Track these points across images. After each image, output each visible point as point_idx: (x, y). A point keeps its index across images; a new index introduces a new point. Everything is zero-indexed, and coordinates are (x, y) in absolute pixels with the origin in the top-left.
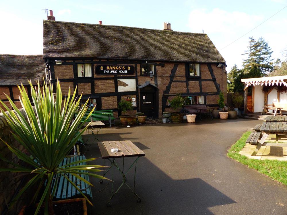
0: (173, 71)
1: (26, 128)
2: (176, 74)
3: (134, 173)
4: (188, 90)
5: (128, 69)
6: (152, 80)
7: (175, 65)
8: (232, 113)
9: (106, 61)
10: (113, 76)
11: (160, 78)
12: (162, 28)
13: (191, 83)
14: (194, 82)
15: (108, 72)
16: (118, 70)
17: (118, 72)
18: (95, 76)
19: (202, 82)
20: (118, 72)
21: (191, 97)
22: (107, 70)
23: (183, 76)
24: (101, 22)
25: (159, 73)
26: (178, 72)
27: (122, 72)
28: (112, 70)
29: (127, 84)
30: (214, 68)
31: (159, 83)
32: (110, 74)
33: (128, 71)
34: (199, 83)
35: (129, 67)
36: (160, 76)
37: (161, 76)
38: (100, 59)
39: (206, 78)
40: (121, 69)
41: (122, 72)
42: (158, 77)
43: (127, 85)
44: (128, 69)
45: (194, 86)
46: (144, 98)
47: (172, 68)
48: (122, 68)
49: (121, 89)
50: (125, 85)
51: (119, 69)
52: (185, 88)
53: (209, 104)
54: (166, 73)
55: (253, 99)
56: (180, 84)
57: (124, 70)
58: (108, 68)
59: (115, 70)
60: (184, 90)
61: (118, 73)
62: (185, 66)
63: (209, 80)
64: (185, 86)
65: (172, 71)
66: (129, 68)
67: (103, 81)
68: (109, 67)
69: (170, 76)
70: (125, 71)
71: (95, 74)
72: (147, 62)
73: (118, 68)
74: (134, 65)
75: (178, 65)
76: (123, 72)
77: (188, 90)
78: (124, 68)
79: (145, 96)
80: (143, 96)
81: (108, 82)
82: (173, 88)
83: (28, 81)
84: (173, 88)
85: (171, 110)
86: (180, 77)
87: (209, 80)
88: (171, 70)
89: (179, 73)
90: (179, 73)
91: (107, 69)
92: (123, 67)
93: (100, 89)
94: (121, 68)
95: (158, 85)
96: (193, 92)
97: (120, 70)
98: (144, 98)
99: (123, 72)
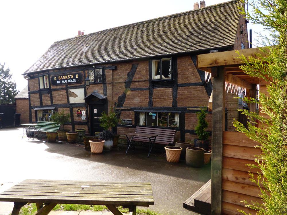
0: (131, 75)
1: (206, 80)
2: (136, 78)
4: (151, 103)
5: (77, 77)
6: (233, 55)
11: (109, 85)
13: (158, 91)
14: (162, 89)
15: (59, 82)
17: (61, 82)
18: (52, 87)
19: (179, 89)
21: (155, 115)
22: (59, 80)
23: (144, 81)
25: (109, 79)
26: (138, 75)
28: (63, 80)
29: (77, 95)
31: (109, 92)
32: (62, 84)
33: (77, 79)
34: (173, 91)
36: (109, 84)
37: (110, 83)
39: (189, 82)
40: (70, 79)
42: (107, 85)
43: (77, 96)
44: (77, 77)
45: (162, 96)
46: (95, 111)
47: (129, 70)
49: (72, 100)
50: (75, 96)
52: (146, 98)
53: (189, 129)
54: (120, 78)
55: (191, 170)
56: (138, 93)
58: (59, 77)
59: (65, 79)
60: (144, 102)
61: (68, 83)
63: (196, 85)
64: (148, 96)
65: (128, 75)
66: (77, 76)
69: (125, 83)
70: (73, 80)
71: (51, 85)
72: (93, 67)
73: (67, 77)
74: (82, 72)
77: (151, 103)
79: (96, 109)
80: (95, 109)
82: (128, 99)
83: (16, 93)
84: (128, 99)
85: (124, 131)
87: (196, 85)
88: (127, 73)
89: (139, 76)
90: (139, 76)
91: (59, 79)
92: (72, 76)
93: (57, 100)
95: (108, 95)
96: (159, 105)
98: (95, 111)
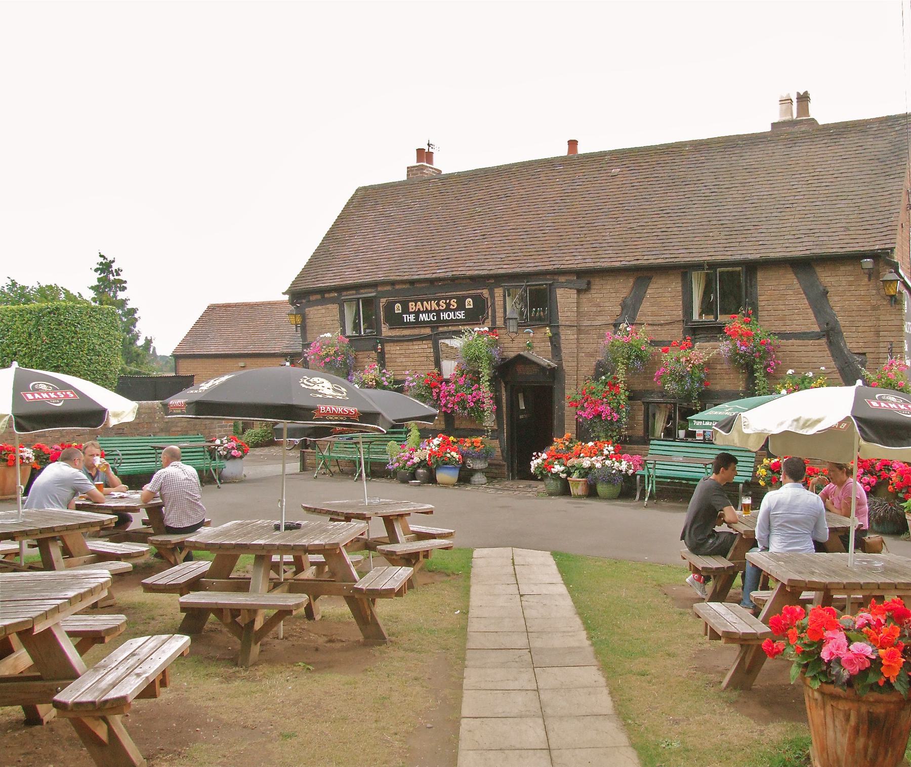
3: (531, 660)
7: (638, 279)
8: (624, 487)
9: (407, 286)
10: (427, 331)
12: (563, 151)
15: (412, 318)
16: (438, 313)
17: (438, 316)
20: (417, 317)
22: (410, 313)
24: (573, 144)
27: (449, 316)
28: (423, 312)
30: (827, 278)
32: (418, 323)
33: (468, 312)
35: (398, 304)
38: (393, 283)
40: (448, 309)
41: (449, 316)
48: (448, 305)
51: (441, 308)
54: (599, 313)
57: (454, 310)
58: (412, 306)
59: (431, 312)
61: (440, 322)
62: (679, 280)
66: (469, 303)
67: (405, 345)
68: (414, 304)
70: (457, 313)
71: (383, 325)
73: (438, 304)
74: (485, 293)
75: (650, 278)
76: (452, 315)
78: (454, 304)
81: (417, 347)
86: (656, 328)
88: (620, 300)
91: (411, 310)
94: (446, 303)
97: (443, 311)
99: (452, 315)
